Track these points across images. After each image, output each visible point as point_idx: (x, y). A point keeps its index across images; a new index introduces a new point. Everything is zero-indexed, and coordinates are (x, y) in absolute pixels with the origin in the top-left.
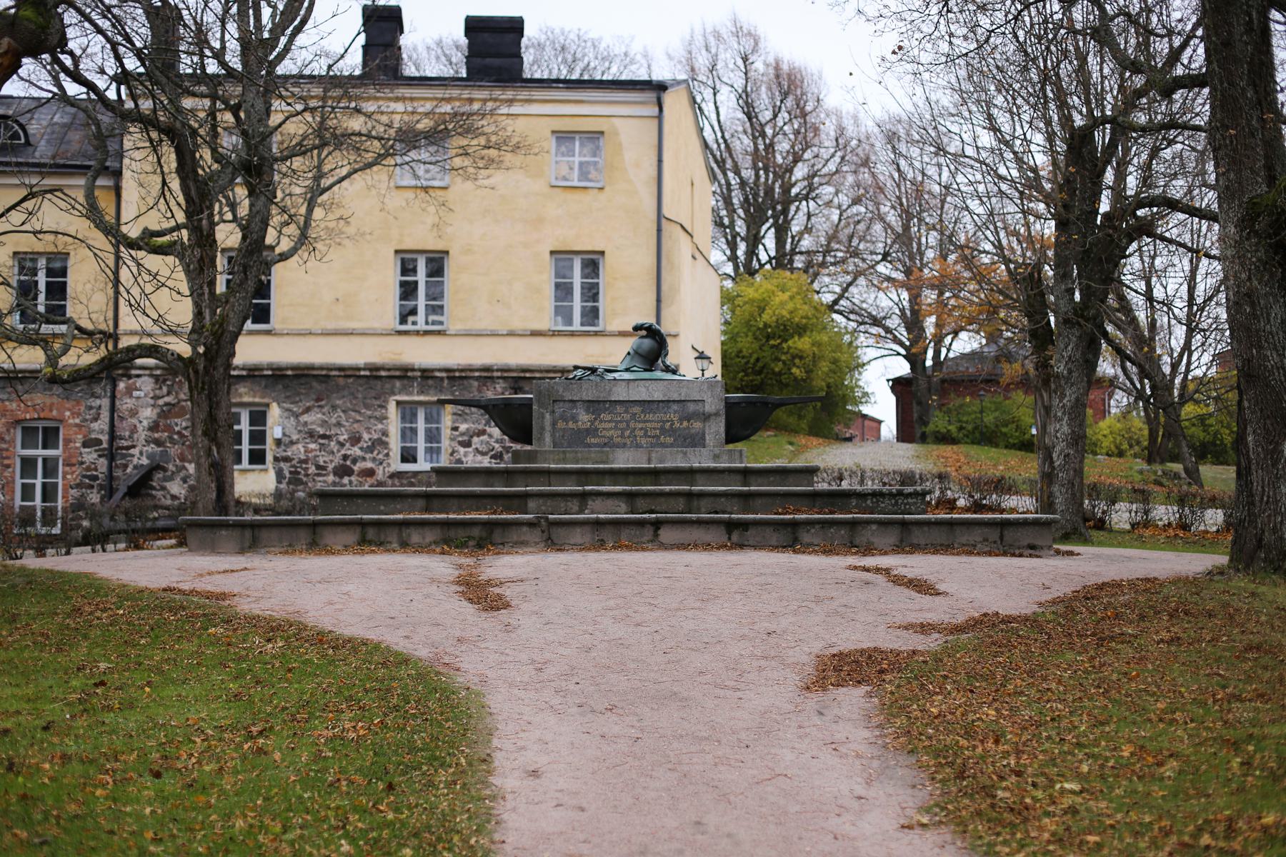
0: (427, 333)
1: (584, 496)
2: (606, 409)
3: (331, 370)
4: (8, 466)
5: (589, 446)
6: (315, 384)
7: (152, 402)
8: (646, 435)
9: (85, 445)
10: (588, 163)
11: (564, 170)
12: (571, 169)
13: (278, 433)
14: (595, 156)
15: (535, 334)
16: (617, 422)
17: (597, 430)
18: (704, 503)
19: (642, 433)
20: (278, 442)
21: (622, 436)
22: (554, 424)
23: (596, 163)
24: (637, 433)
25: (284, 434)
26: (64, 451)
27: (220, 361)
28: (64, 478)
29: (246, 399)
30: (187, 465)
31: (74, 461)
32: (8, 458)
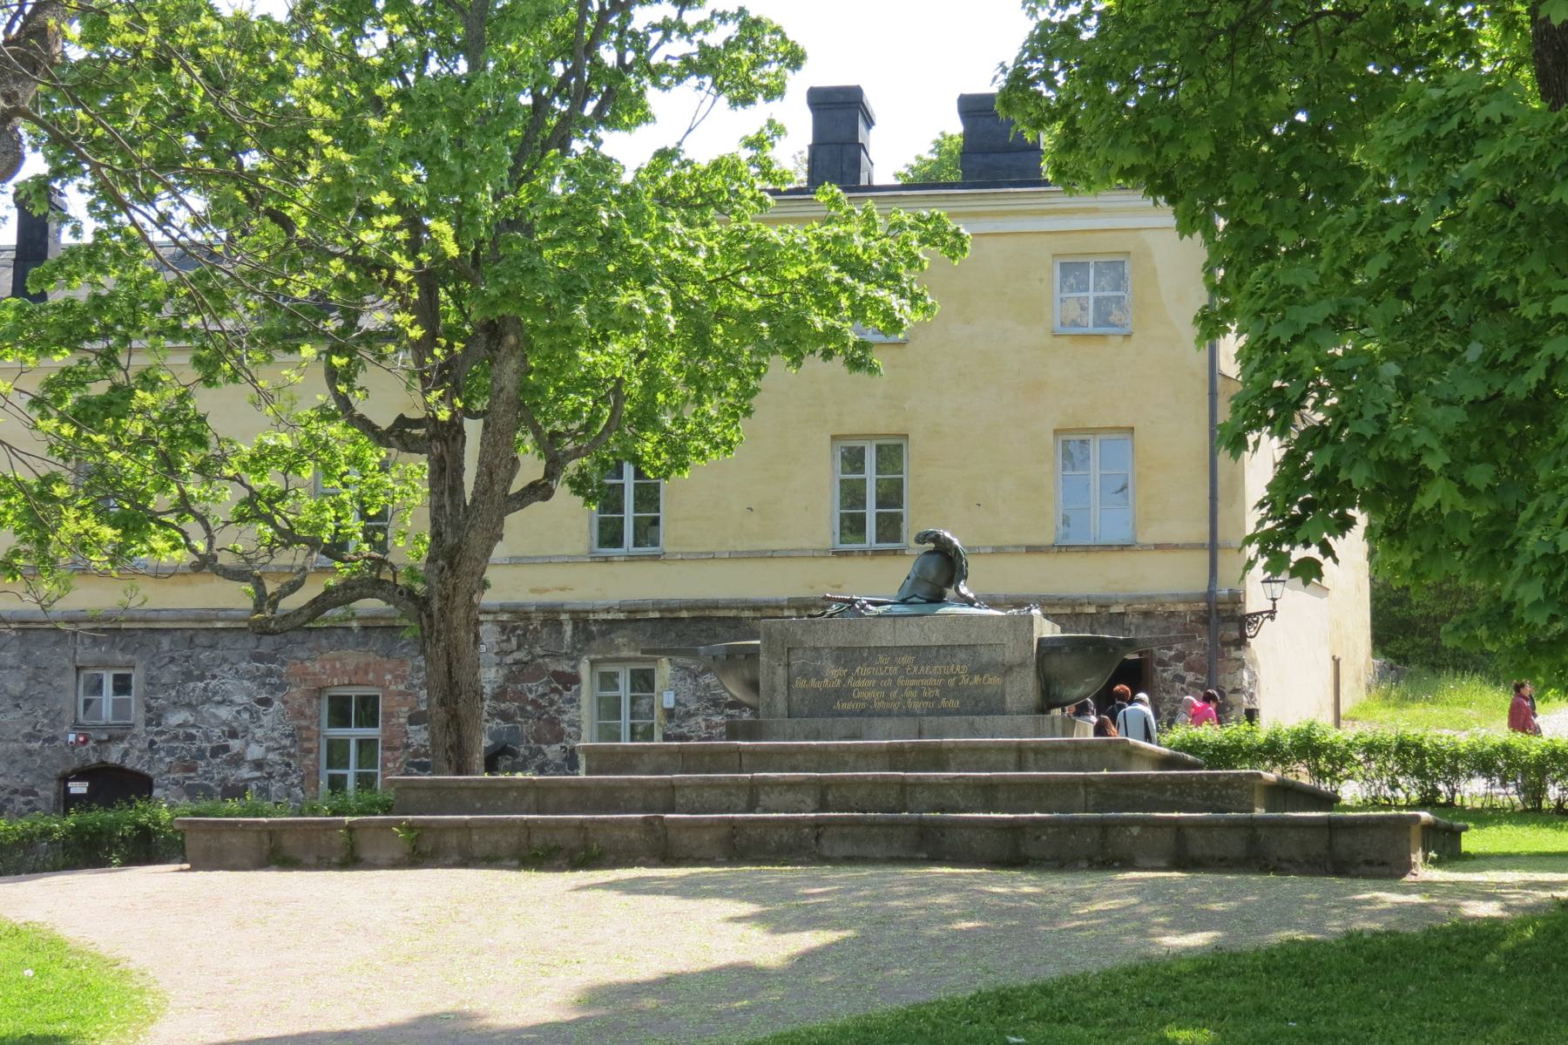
0: (877, 553)
1: (754, 788)
2: (863, 660)
3: (681, 609)
4: (309, 751)
5: (840, 714)
6: (720, 630)
7: (497, 659)
8: (920, 698)
9: (412, 720)
10: (1108, 299)
11: (1073, 312)
12: (1083, 309)
13: (669, 701)
14: (1117, 287)
15: (1032, 549)
16: (878, 679)
17: (850, 690)
18: (775, 797)
19: (914, 694)
20: (670, 714)
21: (886, 699)
22: (789, 683)
23: (1119, 299)
24: (908, 693)
25: (677, 702)
26: (384, 731)
27: (459, 600)
28: (384, 766)
29: (625, 653)
30: (544, 747)
31: (397, 743)
32: (309, 739)
